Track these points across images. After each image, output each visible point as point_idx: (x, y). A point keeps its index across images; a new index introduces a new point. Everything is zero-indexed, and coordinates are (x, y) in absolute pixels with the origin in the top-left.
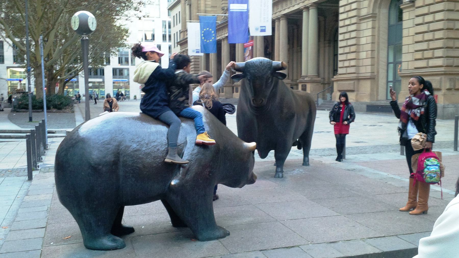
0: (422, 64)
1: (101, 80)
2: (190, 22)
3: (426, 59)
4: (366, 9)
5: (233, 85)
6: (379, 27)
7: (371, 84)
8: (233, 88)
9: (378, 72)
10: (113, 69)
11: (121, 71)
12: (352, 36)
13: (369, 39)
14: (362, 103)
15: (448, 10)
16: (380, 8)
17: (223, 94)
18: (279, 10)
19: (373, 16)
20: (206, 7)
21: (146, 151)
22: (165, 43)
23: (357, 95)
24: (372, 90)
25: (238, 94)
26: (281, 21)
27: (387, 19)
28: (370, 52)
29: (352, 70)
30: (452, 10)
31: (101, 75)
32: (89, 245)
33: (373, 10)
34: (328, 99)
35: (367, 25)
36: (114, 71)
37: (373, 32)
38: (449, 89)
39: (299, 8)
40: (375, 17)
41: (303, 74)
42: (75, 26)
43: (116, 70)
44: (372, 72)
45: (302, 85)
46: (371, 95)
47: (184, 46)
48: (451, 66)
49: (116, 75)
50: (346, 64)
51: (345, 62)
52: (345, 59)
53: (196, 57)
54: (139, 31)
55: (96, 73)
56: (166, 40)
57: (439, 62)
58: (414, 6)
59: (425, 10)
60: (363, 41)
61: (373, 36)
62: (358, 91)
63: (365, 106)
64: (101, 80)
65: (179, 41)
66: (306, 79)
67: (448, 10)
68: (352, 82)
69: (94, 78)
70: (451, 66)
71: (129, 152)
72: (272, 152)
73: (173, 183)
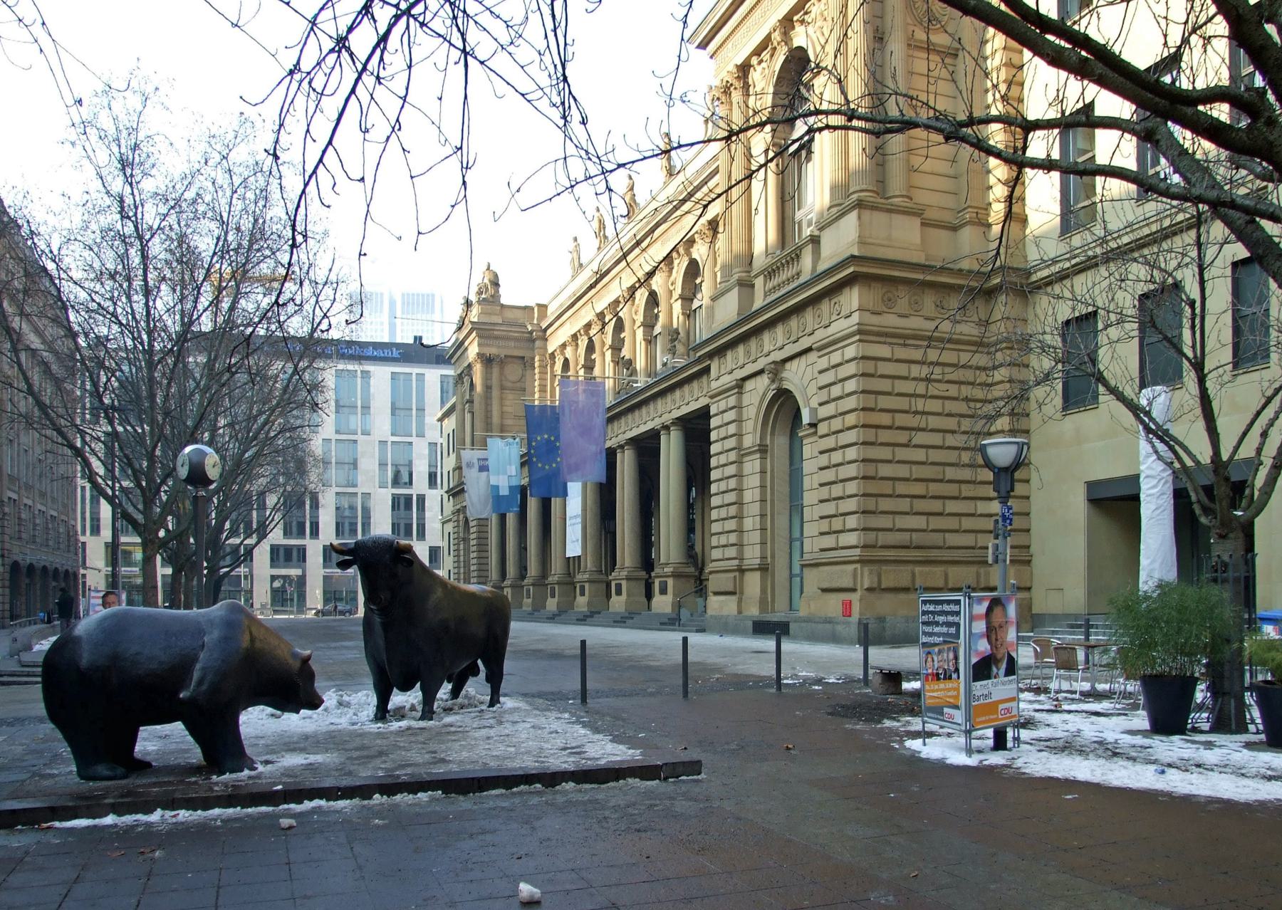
0: (829, 541)
1: (298, 572)
3: (835, 532)
4: (750, 435)
6: (772, 471)
7: (761, 577)
9: (773, 556)
10: (272, 546)
11: (288, 550)
13: (757, 494)
14: (747, 618)
15: (864, 443)
16: (773, 434)
17: (663, 597)
19: (763, 450)
20: (502, 418)
22: (434, 492)
23: (740, 601)
24: (763, 591)
25: (624, 597)
27: (787, 456)
28: (758, 518)
29: (732, 552)
30: (872, 444)
31: (299, 560)
33: (763, 437)
35: (752, 465)
36: (275, 550)
37: (763, 480)
38: (870, 590)
40: (766, 451)
41: (662, 561)
42: (183, 472)
43: (278, 550)
44: (763, 558)
46: (763, 603)
47: (459, 498)
48: (874, 547)
50: (724, 540)
54: (825, 590)
57: (851, 539)
58: (816, 433)
59: (830, 442)
60: (748, 496)
61: (763, 487)
62: (742, 593)
63: (750, 624)
64: (298, 572)
67: (864, 443)
68: (732, 575)
69: (285, 567)
70: (874, 547)
72: (418, 685)
73: (181, 696)
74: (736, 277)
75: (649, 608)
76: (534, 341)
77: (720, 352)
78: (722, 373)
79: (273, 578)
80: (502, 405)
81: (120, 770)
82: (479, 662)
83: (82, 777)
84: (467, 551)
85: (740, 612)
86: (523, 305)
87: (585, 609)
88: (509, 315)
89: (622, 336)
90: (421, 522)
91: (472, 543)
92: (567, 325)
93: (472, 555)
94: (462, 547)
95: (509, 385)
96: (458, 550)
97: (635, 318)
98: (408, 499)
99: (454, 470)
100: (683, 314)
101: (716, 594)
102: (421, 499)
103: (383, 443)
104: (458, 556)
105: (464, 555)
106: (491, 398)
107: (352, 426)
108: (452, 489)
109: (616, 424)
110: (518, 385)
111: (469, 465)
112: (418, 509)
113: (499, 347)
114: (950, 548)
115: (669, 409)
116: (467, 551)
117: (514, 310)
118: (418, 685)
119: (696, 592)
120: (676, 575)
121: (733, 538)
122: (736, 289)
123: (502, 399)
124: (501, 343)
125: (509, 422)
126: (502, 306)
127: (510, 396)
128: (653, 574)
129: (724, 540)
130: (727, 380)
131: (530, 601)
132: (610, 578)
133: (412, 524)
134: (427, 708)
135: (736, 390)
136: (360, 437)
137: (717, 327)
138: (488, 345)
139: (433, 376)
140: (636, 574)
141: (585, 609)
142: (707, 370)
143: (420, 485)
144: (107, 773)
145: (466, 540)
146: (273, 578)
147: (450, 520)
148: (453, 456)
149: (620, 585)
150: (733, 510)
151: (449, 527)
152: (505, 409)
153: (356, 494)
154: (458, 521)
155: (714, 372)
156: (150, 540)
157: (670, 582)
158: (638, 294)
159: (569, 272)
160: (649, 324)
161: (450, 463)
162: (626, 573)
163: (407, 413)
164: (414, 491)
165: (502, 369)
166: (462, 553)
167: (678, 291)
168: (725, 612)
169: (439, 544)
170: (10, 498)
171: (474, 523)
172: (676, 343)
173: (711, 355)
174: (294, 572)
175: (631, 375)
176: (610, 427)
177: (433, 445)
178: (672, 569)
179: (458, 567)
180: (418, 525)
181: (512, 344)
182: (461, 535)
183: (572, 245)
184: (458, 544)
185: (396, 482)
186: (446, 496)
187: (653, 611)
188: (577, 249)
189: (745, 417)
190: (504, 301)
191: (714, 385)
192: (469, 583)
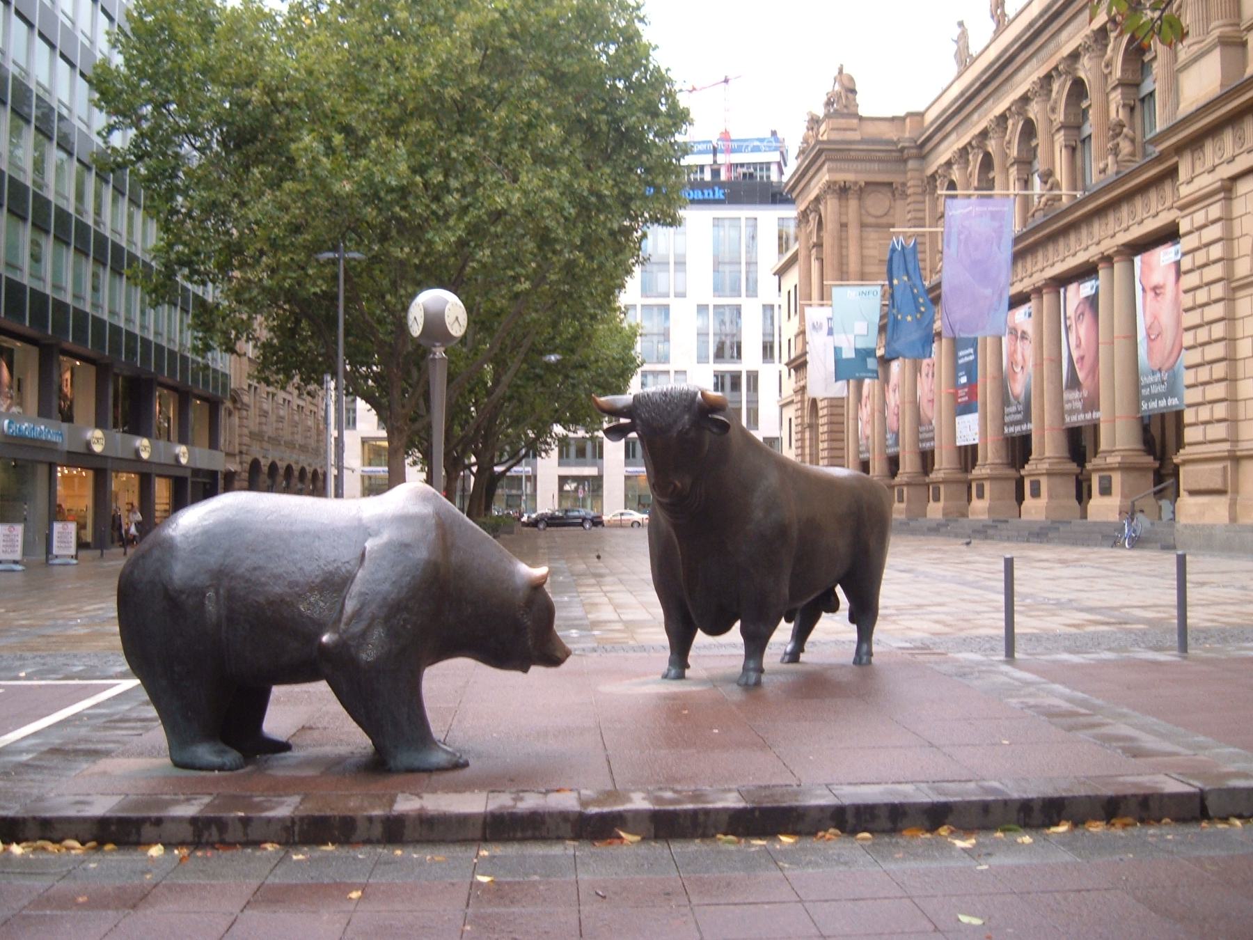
2: (822, 305)
5: (970, 477)
8: (970, 488)
12: (1215, 336)
17: (1106, 500)
18: (1039, 266)
20: (862, 264)
21: (275, 571)
23: (1233, 505)
25: (1043, 501)
26: (1045, 297)
29: (1219, 431)
31: (594, 456)
32: (186, 757)
34: (1166, 515)
39: (1088, 261)
41: (1103, 446)
45: (1101, 478)
49: (634, 456)
50: (1204, 413)
51: (1201, 409)
52: (1200, 399)
53: (835, 403)
55: (581, 453)
56: (772, 356)
62: (1236, 491)
65: (793, 356)
66: (1109, 460)
68: (1219, 466)
69: (577, 465)
71: (243, 570)
72: (738, 624)
74: (1216, 33)
75: (1084, 515)
76: (905, 161)
77: (1195, 143)
78: (1197, 172)
79: (563, 480)
80: (862, 247)
81: (232, 756)
82: (839, 590)
83: (177, 765)
84: (815, 441)
85: (1233, 519)
86: (890, 115)
87: (985, 517)
88: (871, 130)
89: (1033, 144)
90: (753, 406)
91: (821, 429)
92: (953, 137)
93: (821, 446)
94: (807, 435)
95: (871, 220)
96: (803, 440)
97: (1053, 117)
98: (736, 379)
99: (796, 336)
100: (1124, 106)
101: (1193, 493)
102: (753, 377)
103: (702, 309)
104: (803, 447)
105: (811, 446)
106: (847, 239)
107: (662, 288)
108: (795, 359)
109: (1029, 260)
110: (884, 220)
111: (816, 327)
112: (748, 389)
113: (856, 172)
114: (1212, 442)
115: (1111, 232)
116: (815, 441)
117: (877, 123)
118: (738, 624)
119: (1155, 493)
120: (1125, 468)
121: (1220, 411)
122: (1216, 54)
123: (861, 239)
124: (860, 166)
125: (868, 269)
126: (861, 119)
127: (872, 235)
128: (1089, 466)
129: (1204, 413)
130: (1206, 182)
131: (903, 505)
132: (1023, 472)
133: (740, 409)
134: (752, 664)
135: (1222, 195)
136: (671, 301)
137: (1186, 108)
138: (841, 170)
139: (769, 219)
140: (1061, 467)
141: (985, 517)
142: (1172, 173)
143: (751, 359)
144: (215, 759)
145: (813, 427)
146: (563, 480)
147: (792, 402)
148: (795, 320)
149: (1038, 482)
150: (1220, 370)
151: (790, 412)
152: (866, 252)
153: (668, 372)
154: (802, 401)
155: (1183, 174)
156: (398, 428)
157: (1117, 478)
158: (1055, 86)
159: (954, 69)
160: (1074, 125)
161: (789, 329)
162: (1046, 466)
163: (735, 268)
164: (743, 366)
165: (860, 199)
166: (807, 443)
167: (1060, 117)
168: (1208, 520)
169: (775, 434)
170: (298, 406)
171: (825, 403)
172: (1119, 139)
173: (1179, 149)
174: (590, 471)
175: (1051, 189)
176: (1020, 265)
177: (768, 309)
178: (1119, 459)
179: (802, 417)
180: (748, 410)
181: (876, 166)
182: (807, 420)
183: (958, 31)
184: (802, 432)
185: (719, 355)
186: (785, 370)
187: (1089, 519)
188: (963, 36)
189: (1237, 233)
190: (863, 112)
191: (1184, 190)
192: (818, 464)
